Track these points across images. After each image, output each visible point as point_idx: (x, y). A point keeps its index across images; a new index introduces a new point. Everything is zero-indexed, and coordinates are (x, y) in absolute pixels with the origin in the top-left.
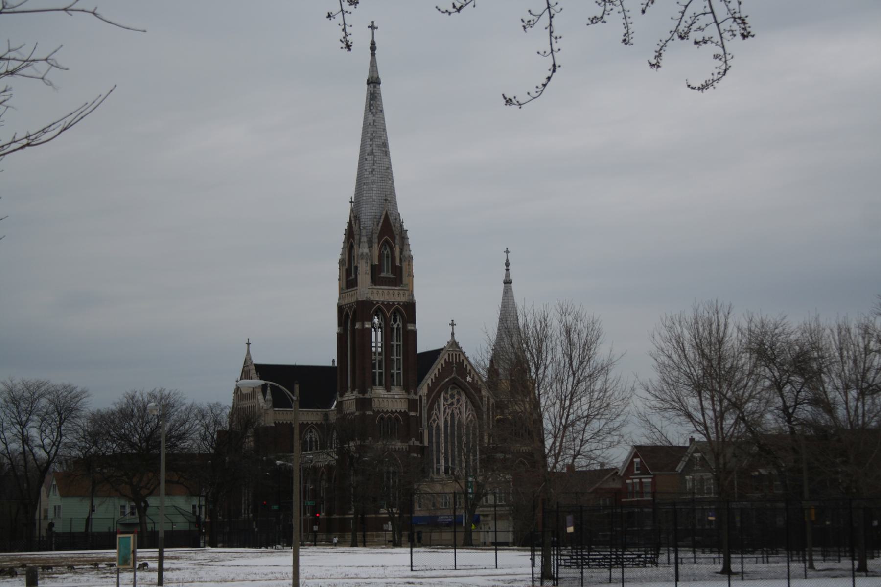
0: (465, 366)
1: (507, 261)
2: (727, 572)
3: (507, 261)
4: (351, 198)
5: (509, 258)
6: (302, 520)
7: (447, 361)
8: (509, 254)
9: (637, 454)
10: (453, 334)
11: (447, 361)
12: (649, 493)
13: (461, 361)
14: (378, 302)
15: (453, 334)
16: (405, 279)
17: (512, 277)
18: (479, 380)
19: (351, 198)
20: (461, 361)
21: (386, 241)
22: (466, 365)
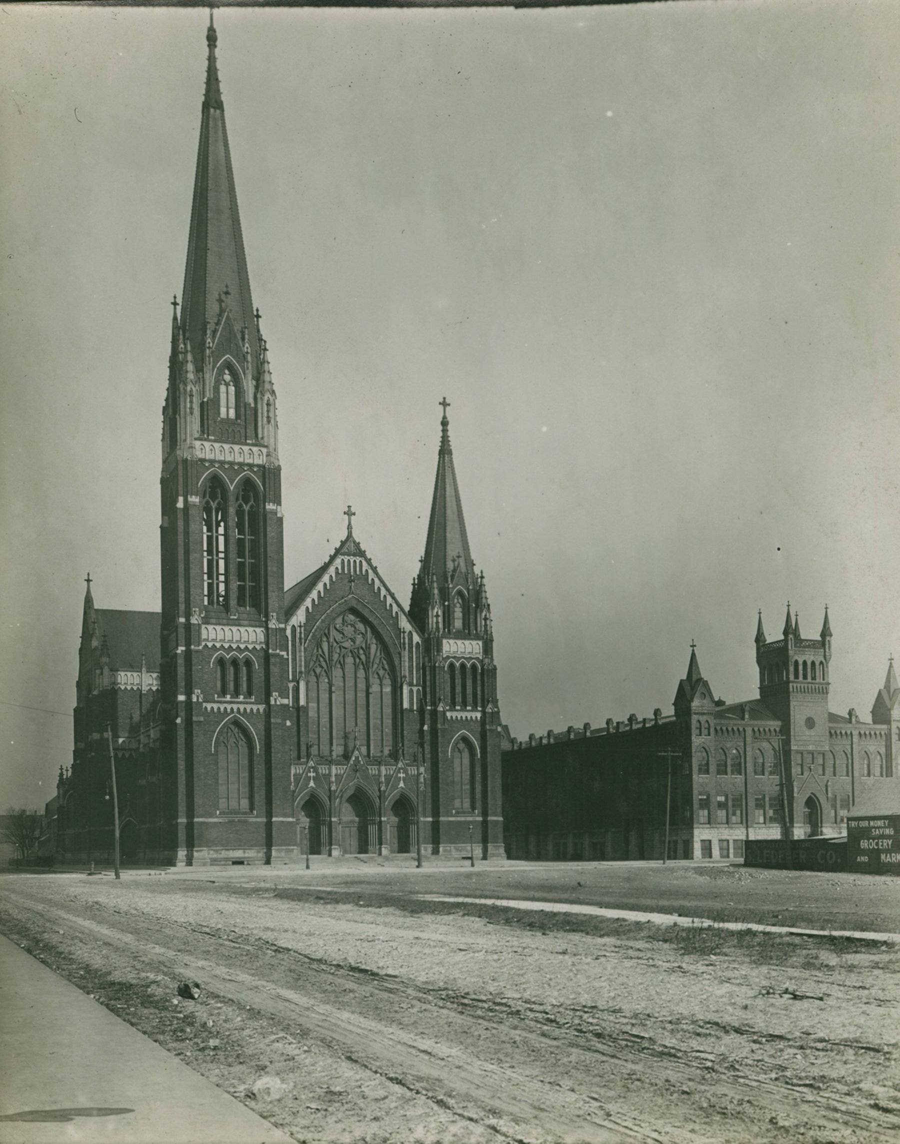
0: (382, 599)
1: (444, 417)
2: (544, 934)
3: (444, 417)
4: (175, 297)
5: (447, 415)
6: (182, 808)
7: (340, 571)
8: (448, 408)
9: (743, 711)
10: (350, 527)
11: (340, 571)
12: (747, 836)
13: (364, 573)
14: (212, 462)
15: (350, 527)
16: (265, 431)
17: (449, 419)
18: (370, 571)
19: (175, 297)
20: (364, 573)
21: (229, 366)
22: (391, 605)
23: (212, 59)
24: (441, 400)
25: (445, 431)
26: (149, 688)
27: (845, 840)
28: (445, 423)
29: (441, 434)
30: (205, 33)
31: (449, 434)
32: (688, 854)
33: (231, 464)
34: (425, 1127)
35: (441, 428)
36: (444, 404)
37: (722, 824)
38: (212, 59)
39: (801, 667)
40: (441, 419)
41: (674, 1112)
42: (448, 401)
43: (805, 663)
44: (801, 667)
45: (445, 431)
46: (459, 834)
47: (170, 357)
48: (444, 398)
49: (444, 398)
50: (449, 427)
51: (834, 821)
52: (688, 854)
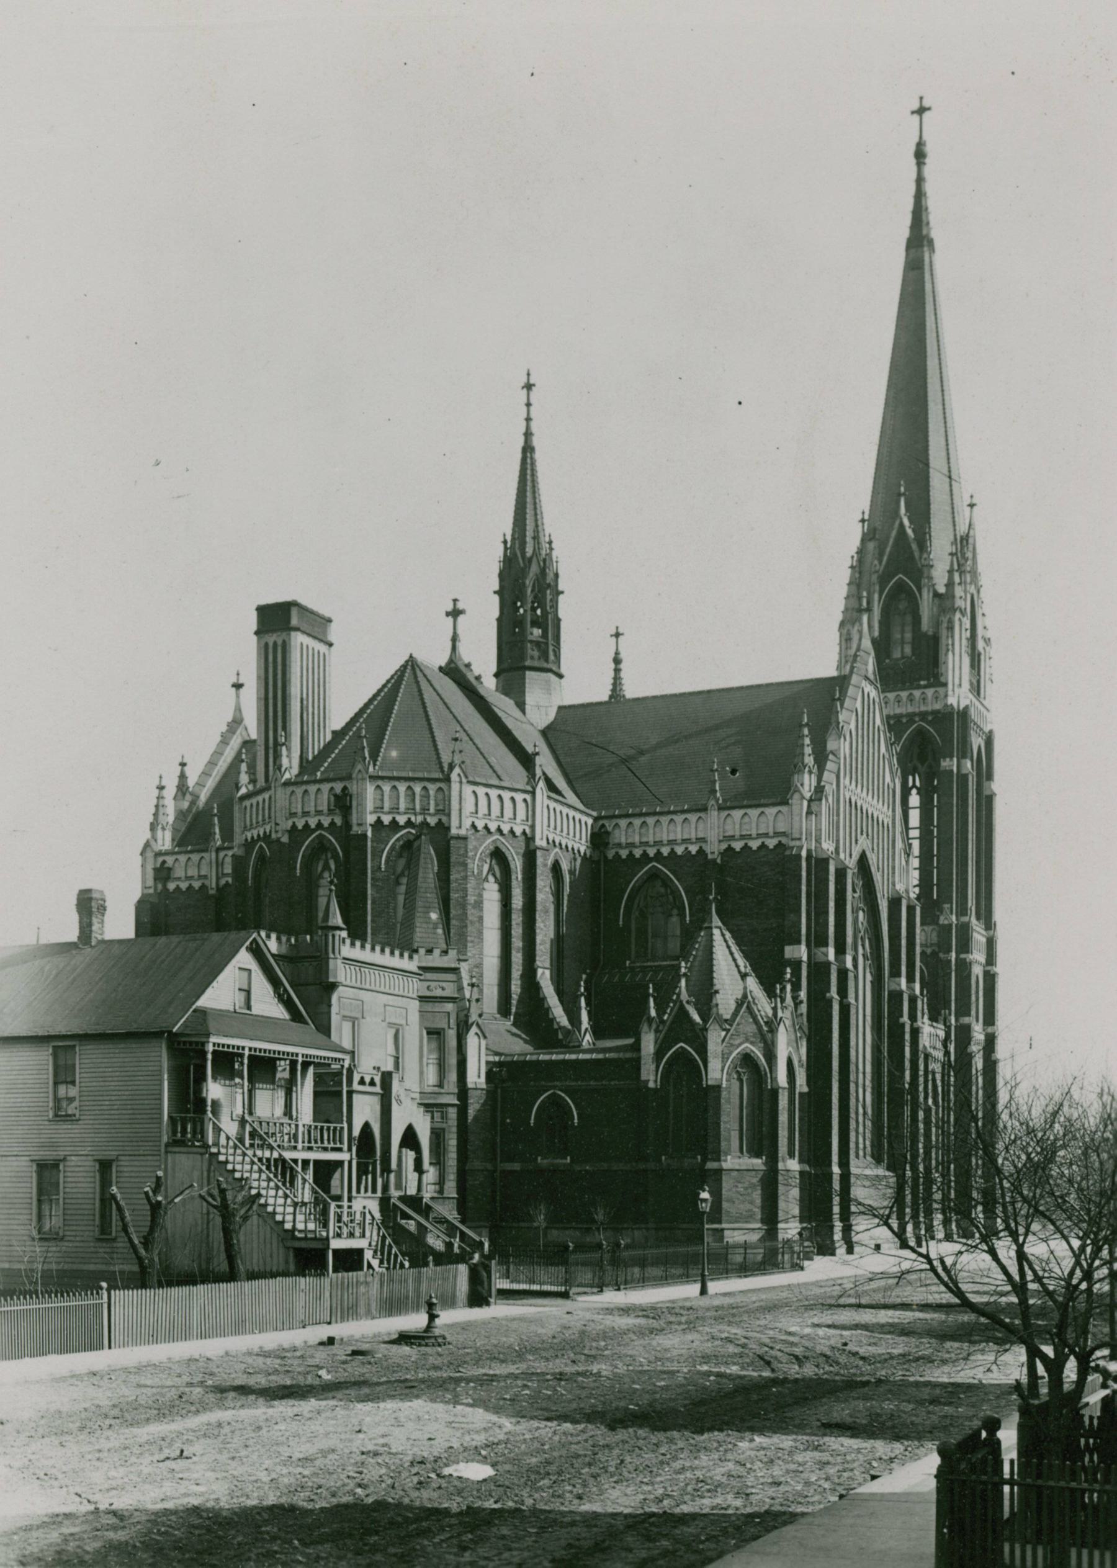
1: (617, 653)
3: (617, 653)
8: (461, 618)
17: (623, 655)
23: (920, 180)
25: (617, 671)
26: (724, 846)
28: (617, 661)
29: (612, 674)
30: (913, 148)
31: (623, 674)
32: (361, 1269)
35: (613, 666)
37: (303, 805)
38: (920, 180)
39: (271, 650)
40: (613, 655)
43: (275, 643)
44: (271, 650)
45: (617, 671)
47: (499, 620)
50: (622, 666)
52: (361, 1269)
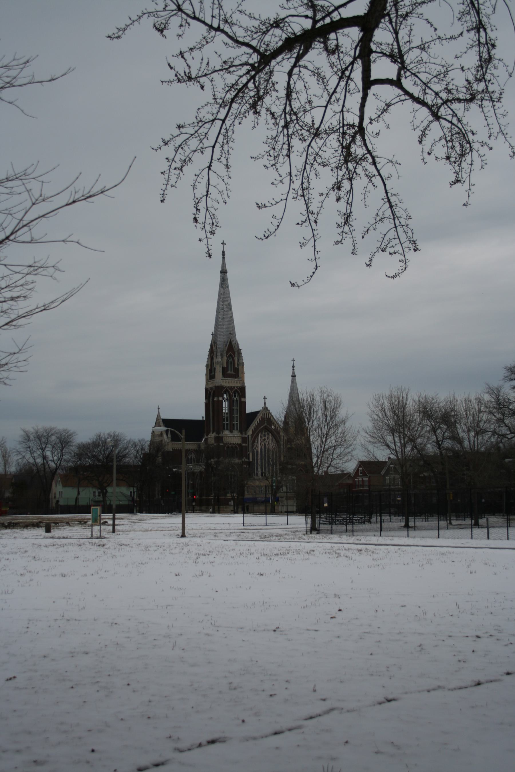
1: (293, 365)
3: (293, 365)
8: (225, 246)
10: (265, 403)
15: (265, 403)
16: (240, 375)
17: (295, 365)
24: (222, 242)
27: (101, 507)
28: (293, 367)
30: (222, 253)
33: (231, 387)
34: (284, 553)
36: (223, 244)
41: (435, 400)
42: (225, 242)
46: (442, 520)
48: (223, 241)
49: (223, 241)
51: (180, 532)
